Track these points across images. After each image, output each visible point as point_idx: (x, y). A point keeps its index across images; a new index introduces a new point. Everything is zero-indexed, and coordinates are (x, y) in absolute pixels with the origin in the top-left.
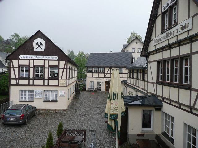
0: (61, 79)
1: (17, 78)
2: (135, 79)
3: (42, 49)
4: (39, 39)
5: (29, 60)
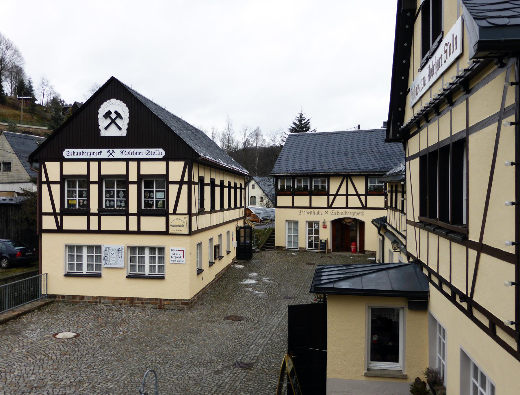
0: (174, 213)
1: (58, 211)
3: (120, 129)
4: (113, 101)
5: (88, 161)
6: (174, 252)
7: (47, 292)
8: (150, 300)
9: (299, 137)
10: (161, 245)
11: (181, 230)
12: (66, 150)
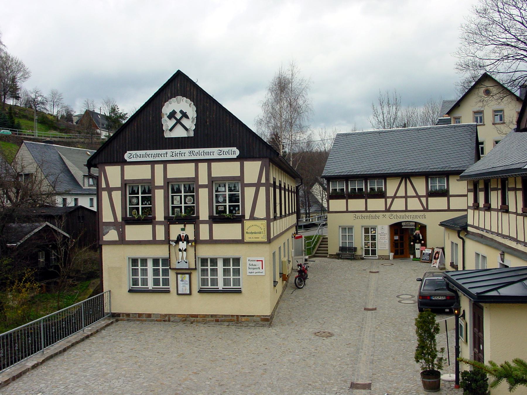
2: (494, 214)
3: (186, 129)
5: (153, 163)
6: (251, 263)
7: (110, 310)
8: (225, 317)
9: (348, 136)
10: (236, 255)
11: (259, 238)
12: (128, 152)
